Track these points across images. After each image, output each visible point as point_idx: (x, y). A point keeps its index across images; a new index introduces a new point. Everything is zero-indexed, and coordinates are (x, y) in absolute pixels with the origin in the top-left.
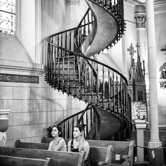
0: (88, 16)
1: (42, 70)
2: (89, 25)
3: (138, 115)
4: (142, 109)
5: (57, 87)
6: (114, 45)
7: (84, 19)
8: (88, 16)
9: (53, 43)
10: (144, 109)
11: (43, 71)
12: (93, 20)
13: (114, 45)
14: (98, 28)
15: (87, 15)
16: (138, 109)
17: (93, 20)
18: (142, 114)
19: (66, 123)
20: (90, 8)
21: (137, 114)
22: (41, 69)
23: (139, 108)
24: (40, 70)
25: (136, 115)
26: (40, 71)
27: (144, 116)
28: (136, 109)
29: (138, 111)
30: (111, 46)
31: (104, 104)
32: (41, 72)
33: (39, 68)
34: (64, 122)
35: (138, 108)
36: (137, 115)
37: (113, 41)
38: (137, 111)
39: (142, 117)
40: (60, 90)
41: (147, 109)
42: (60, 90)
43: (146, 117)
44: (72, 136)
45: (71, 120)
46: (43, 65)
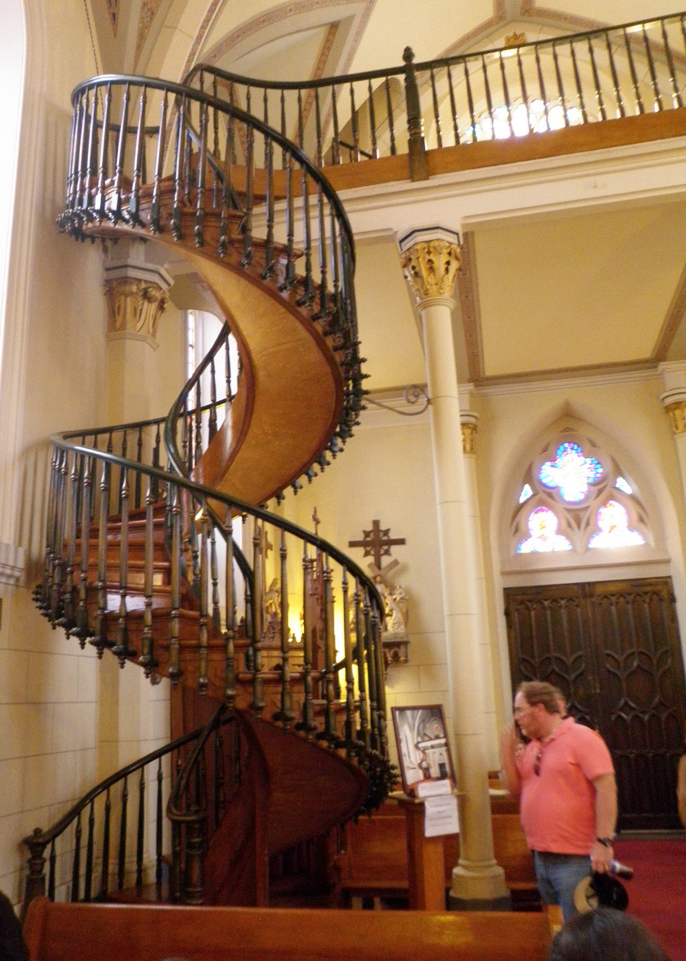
0: (213, 372)
1: (17, 574)
2: (214, 400)
3: (424, 765)
4: (431, 739)
5: (91, 635)
6: (310, 481)
7: (210, 365)
8: (213, 372)
9: (147, 138)
10: (437, 737)
11: (18, 579)
12: (234, 391)
13: (310, 481)
14: (255, 416)
15: (209, 367)
16: (420, 740)
17: (234, 391)
18: (437, 757)
19: (100, 802)
20: (230, 324)
21: (419, 761)
22: (13, 568)
23: (424, 736)
24: (8, 571)
25: (416, 765)
26: (10, 576)
27: (442, 766)
28: (413, 738)
29: (421, 745)
30: (323, 463)
31: (332, 721)
32: (12, 581)
33: (7, 559)
34: (92, 801)
35: (418, 734)
36: (420, 765)
37: (304, 467)
38: (416, 746)
39: (435, 772)
40: (106, 651)
41: (446, 736)
42: (106, 651)
43: (448, 769)
44: (135, 867)
45: (117, 788)
46: (22, 551)
